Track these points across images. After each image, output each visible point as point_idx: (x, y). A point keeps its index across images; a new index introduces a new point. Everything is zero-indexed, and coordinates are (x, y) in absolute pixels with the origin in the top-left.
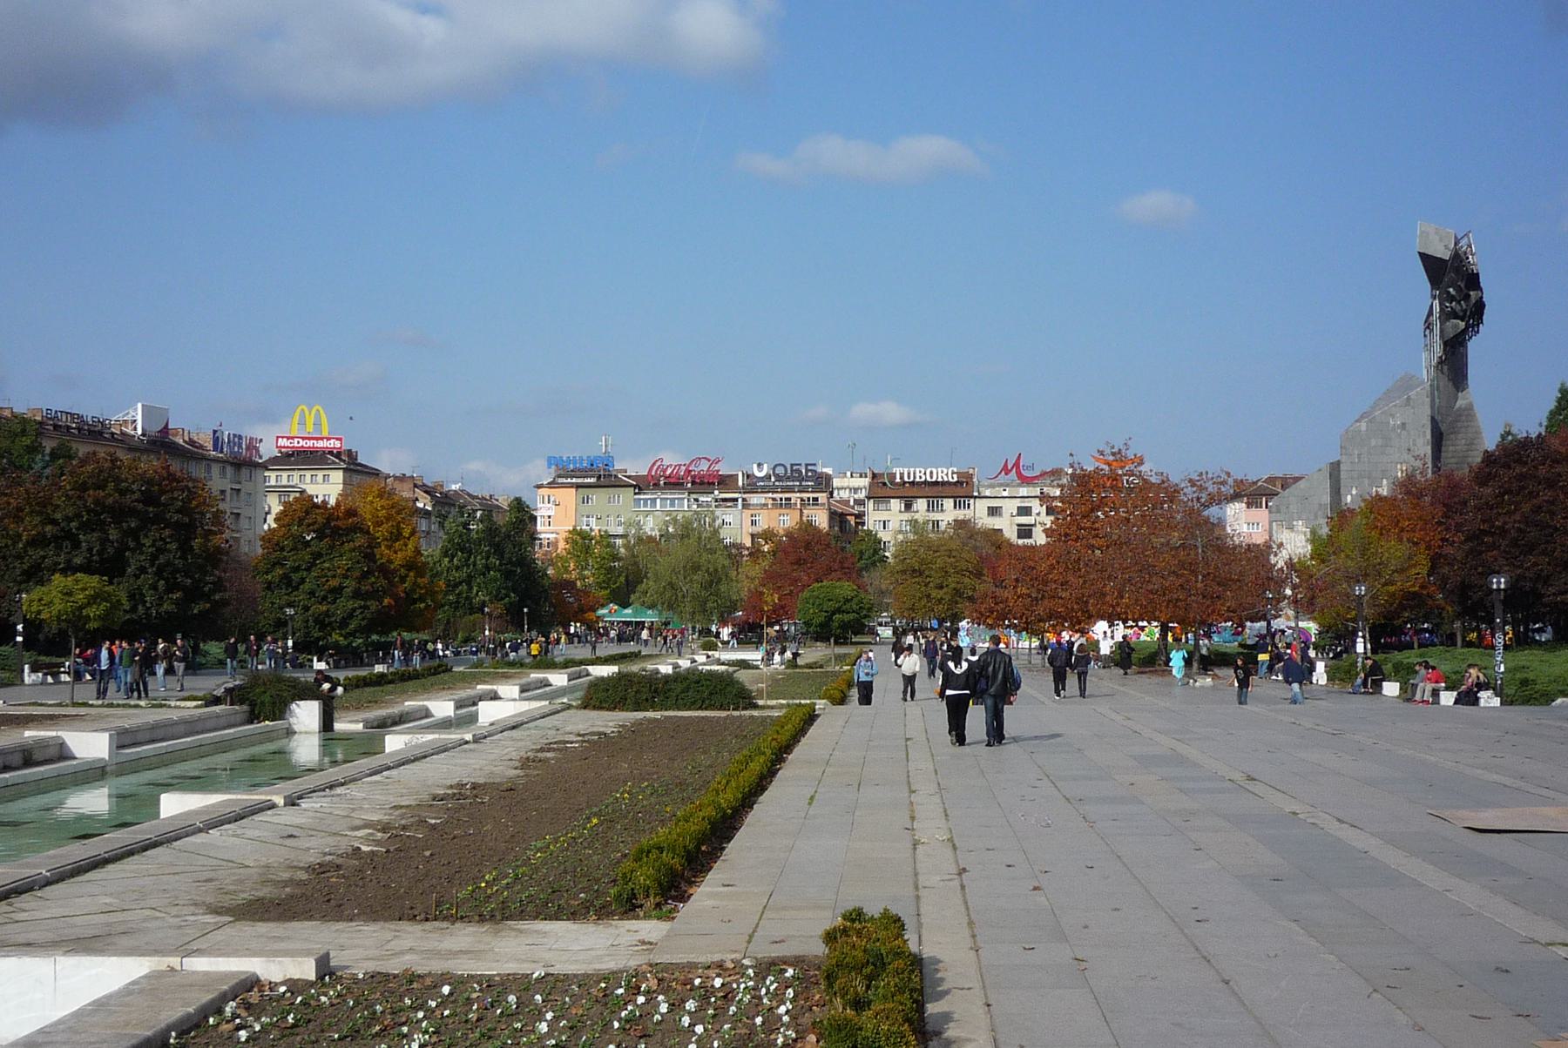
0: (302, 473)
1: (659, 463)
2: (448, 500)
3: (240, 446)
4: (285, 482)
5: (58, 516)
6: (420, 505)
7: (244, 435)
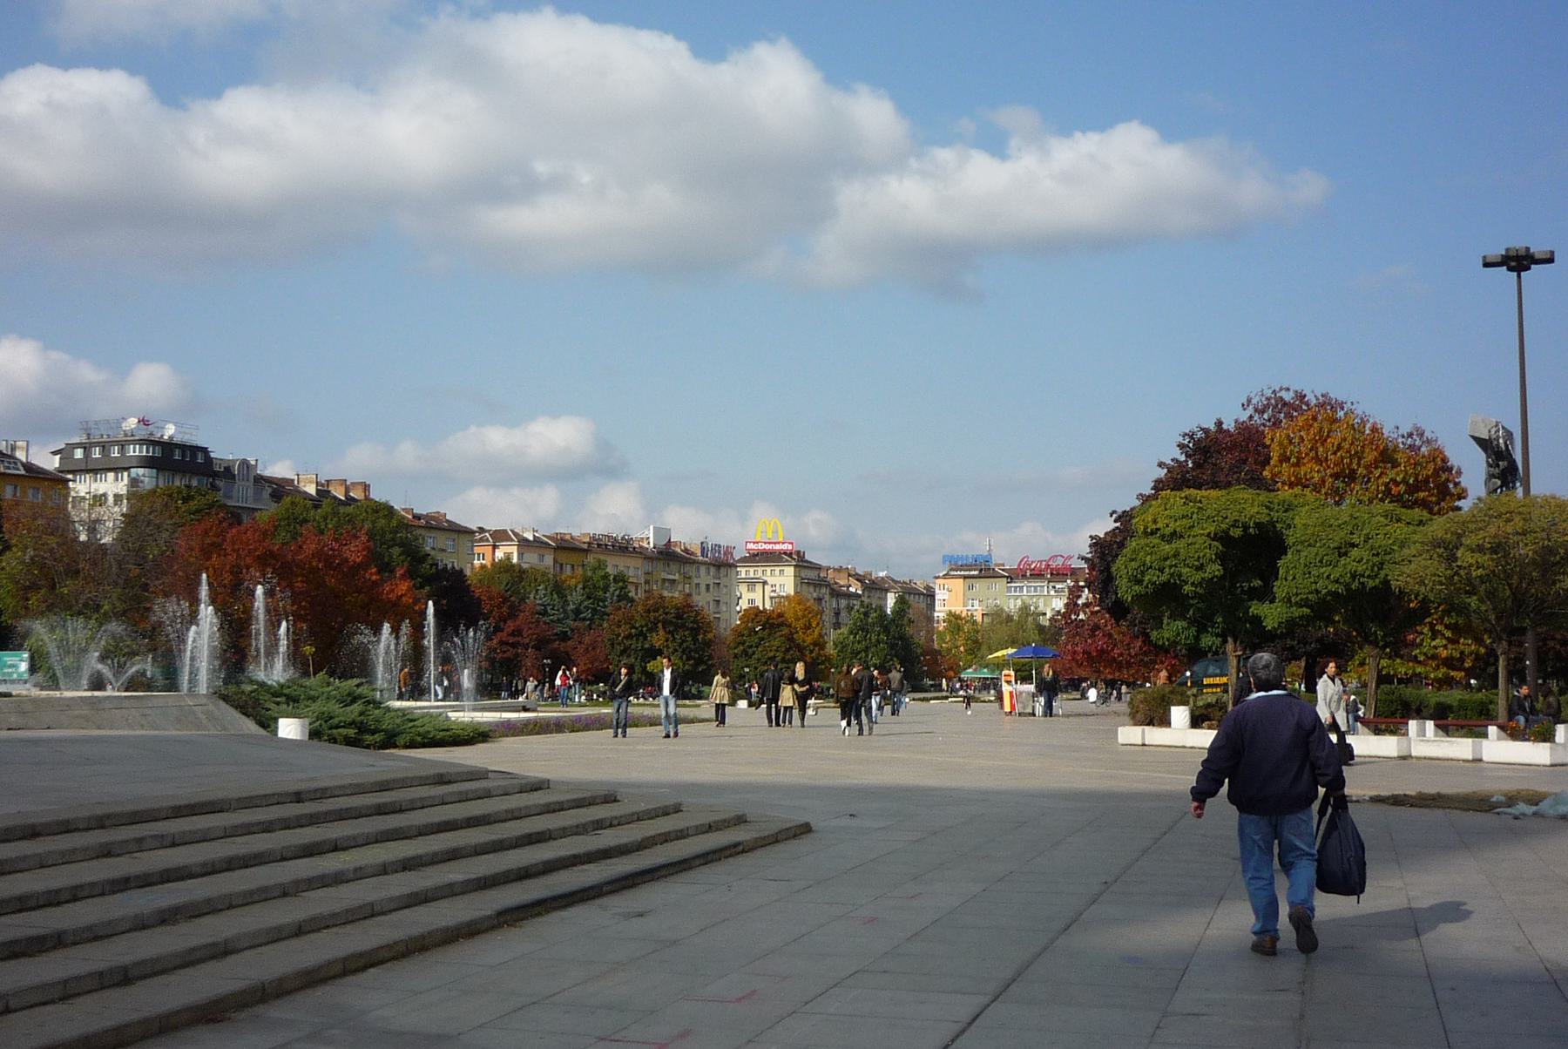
0: (764, 568)
1: (1026, 559)
2: (874, 586)
3: (720, 552)
4: (752, 575)
5: (637, 625)
6: (852, 590)
7: (722, 545)
